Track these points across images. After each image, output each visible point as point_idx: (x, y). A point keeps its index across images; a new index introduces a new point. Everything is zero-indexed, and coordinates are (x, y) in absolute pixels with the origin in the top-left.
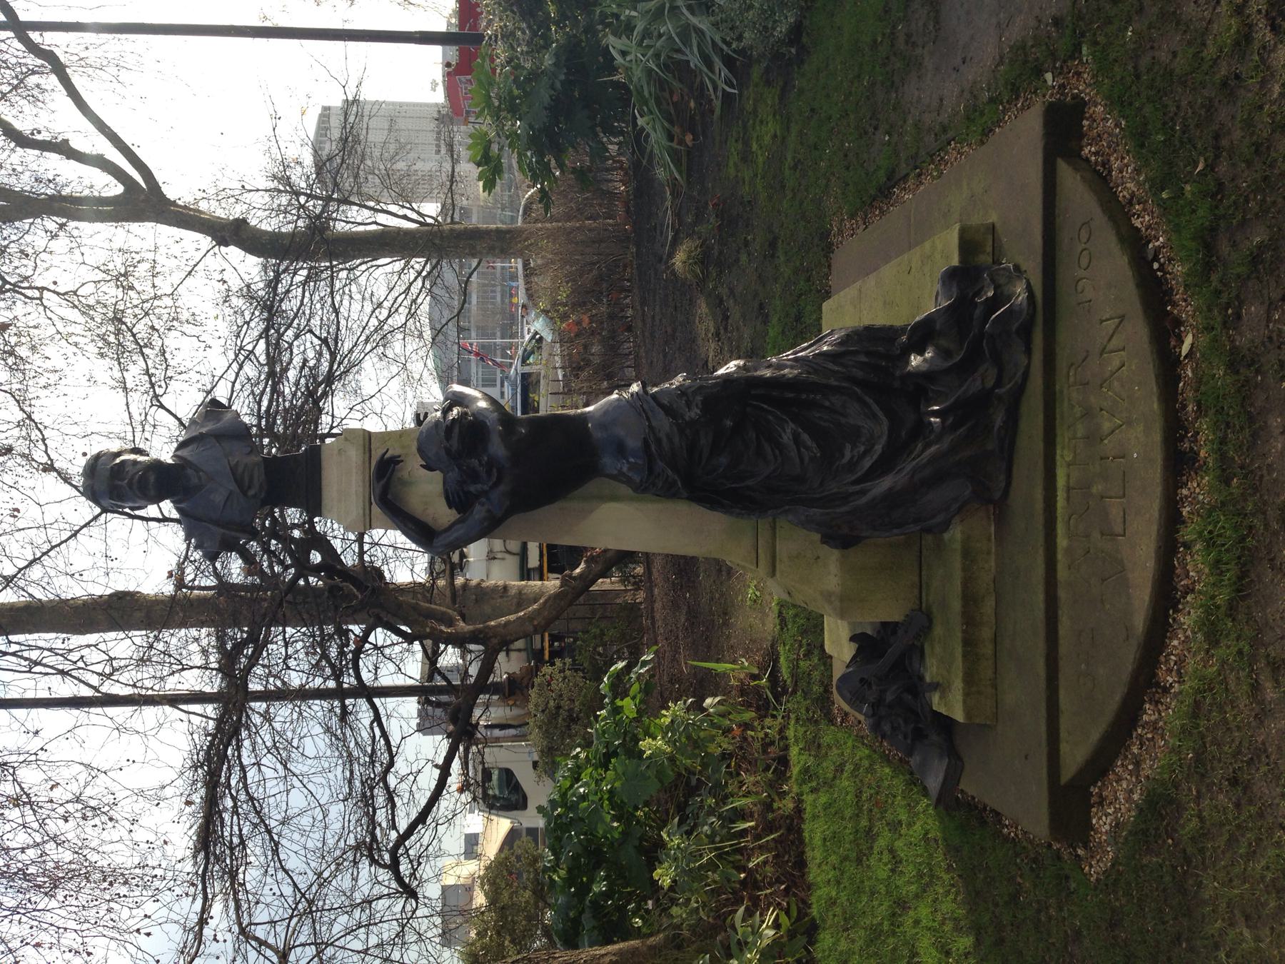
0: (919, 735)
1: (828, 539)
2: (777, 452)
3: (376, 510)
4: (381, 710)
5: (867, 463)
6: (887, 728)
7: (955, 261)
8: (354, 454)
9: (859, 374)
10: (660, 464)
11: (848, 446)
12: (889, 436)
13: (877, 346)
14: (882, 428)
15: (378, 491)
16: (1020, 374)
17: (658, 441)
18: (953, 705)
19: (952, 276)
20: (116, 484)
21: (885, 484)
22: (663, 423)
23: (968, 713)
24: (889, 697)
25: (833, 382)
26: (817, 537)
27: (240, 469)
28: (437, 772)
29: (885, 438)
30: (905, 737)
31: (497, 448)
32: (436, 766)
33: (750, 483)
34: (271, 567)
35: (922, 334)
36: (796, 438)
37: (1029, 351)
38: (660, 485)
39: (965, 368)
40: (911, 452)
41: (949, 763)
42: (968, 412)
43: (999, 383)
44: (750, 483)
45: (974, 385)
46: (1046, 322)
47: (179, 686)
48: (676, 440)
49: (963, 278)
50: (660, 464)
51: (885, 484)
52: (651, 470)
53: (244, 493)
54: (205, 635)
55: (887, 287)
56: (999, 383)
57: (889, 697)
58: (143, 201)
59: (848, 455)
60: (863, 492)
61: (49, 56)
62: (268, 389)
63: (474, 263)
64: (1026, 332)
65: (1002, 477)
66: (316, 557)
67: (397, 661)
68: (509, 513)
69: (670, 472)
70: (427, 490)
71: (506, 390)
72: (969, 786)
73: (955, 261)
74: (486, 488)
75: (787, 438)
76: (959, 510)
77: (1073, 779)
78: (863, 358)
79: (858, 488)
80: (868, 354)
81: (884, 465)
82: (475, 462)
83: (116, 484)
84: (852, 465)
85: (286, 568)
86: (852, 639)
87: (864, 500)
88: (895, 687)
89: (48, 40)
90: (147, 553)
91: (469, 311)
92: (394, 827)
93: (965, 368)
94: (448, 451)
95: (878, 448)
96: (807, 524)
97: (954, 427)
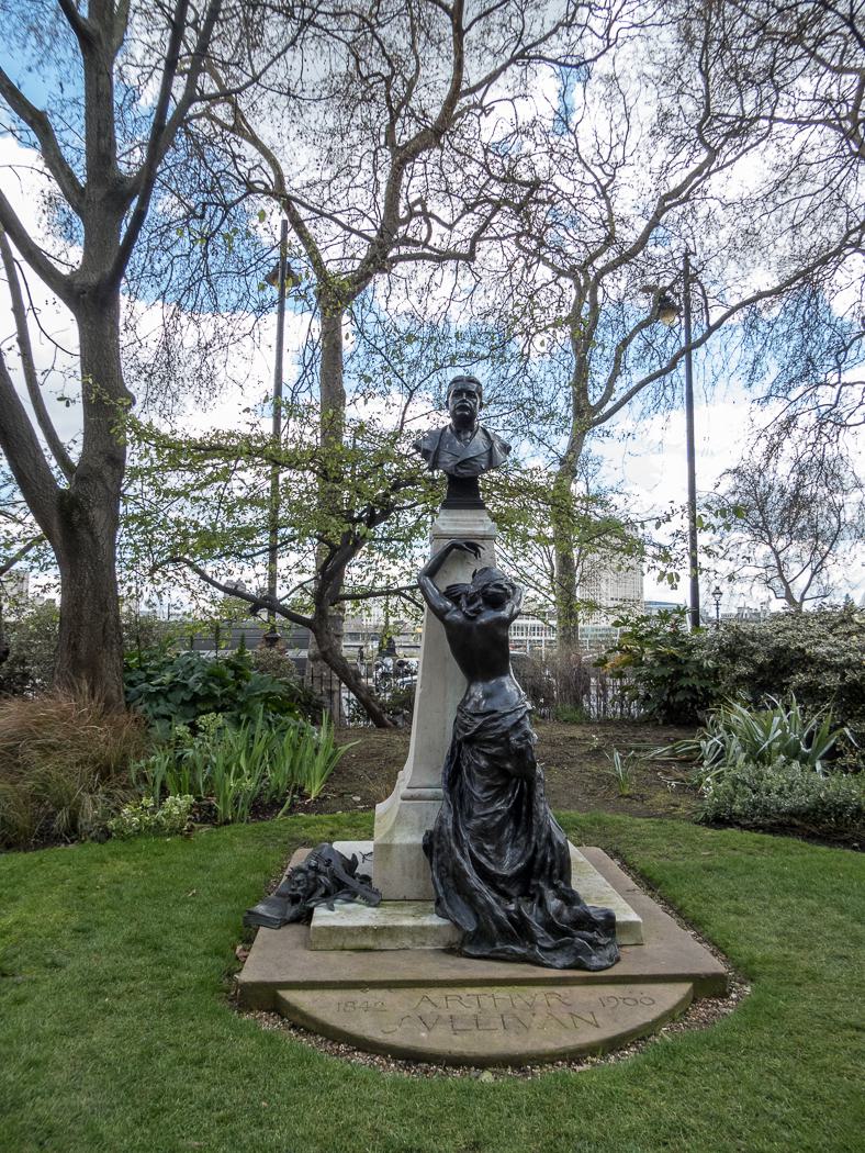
3: (447, 542)
5: (483, 859)
6: (300, 877)
9: (539, 856)
10: (479, 721)
11: (493, 848)
13: (556, 869)
14: (506, 871)
15: (459, 542)
17: (495, 720)
18: (323, 917)
19: (610, 917)
21: (467, 866)
22: (509, 721)
23: (315, 928)
24: (322, 878)
25: (533, 838)
26: (431, 826)
31: (488, 616)
33: (467, 781)
35: (570, 899)
36: (498, 812)
37: (565, 968)
39: (549, 926)
43: (543, 949)
45: (539, 932)
46: (588, 978)
48: (499, 731)
50: (479, 721)
52: (475, 715)
55: (596, 883)
56: (543, 949)
57: (322, 878)
58: (586, 416)
59: (488, 847)
61: (673, 365)
64: (579, 966)
65: (478, 953)
67: (297, 569)
75: (498, 806)
76: (456, 924)
79: (467, 853)
80: (553, 862)
82: (481, 601)
84: (481, 850)
86: (354, 856)
87: (459, 857)
89: (682, 369)
96: (441, 820)
97: (511, 919)
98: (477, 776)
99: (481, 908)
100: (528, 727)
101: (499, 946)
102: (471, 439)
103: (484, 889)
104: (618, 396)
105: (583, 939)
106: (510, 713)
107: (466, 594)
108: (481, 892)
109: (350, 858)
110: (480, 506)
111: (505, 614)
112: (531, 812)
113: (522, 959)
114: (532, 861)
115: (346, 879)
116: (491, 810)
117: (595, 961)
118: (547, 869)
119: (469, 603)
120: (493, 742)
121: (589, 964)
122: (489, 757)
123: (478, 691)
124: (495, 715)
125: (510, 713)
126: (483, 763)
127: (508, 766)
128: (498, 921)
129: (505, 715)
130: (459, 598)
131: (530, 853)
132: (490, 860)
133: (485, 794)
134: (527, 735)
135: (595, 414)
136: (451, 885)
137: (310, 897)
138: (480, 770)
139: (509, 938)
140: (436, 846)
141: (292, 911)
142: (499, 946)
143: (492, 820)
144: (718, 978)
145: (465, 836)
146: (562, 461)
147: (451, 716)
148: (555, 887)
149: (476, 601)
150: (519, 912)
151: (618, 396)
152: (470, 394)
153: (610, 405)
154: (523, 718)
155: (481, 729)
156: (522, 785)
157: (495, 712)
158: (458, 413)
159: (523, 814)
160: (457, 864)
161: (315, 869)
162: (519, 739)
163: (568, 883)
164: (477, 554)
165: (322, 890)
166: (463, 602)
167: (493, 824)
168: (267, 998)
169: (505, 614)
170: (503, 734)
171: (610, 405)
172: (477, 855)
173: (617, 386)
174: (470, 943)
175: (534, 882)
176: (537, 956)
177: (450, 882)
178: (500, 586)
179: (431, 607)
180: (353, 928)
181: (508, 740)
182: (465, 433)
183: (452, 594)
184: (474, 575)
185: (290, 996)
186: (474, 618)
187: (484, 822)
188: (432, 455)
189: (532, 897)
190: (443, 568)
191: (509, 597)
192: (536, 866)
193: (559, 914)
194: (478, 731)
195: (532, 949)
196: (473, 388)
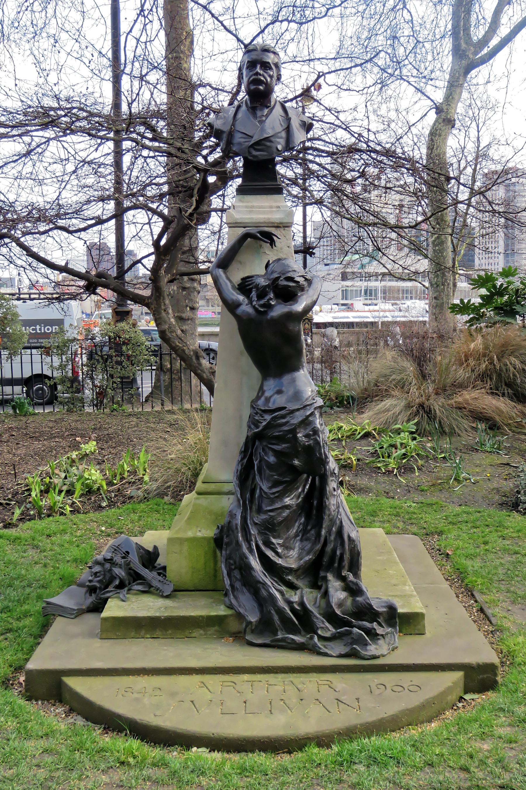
0: (92, 590)
1: (221, 529)
2: (277, 495)
3: (241, 231)
4: (106, 225)
5: (270, 554)
7: (400, 610)
8: (277, 217)
10: (268, 417)
12: (287, 568)
16: (326, 651)
17: (283, 417)
19: (392, 609)
20: (258, 69)
21: (255, 563)
22: (298, 417)
25: (323, 532)
26: (223, 521)
27: (268, 144)
28: (63, 264)
29: (286, 565)
30: (90, 581)
31: (279, 310)
32: (67, 263)
34: (206, 148)
35: (354, 591)
36: (287, 507)
38: (256, 418)
39: (331, 617)
40: (276, 582)
41: (74, 610)
42: (304, 620)
44: (257, 478)
47: (199, 651)
48: (286, 428)
49: (393, 617)
50: (268, 417)
51: (255, 563)
52: (265, 411)
53: (252, 146)
54: (162, 98)
55: (391, 568)
56: (321, 638)
60: (251, 551)
62: (317, 160)
63: (427, 284)
64: (352, 654)
66: (212, 179)
67: (142, 235)
68: (238, 318)
69: (264, 423)
70: (254, 266)
71: (450, 255)
72: (59, 624)
73: (400, 610)
74: (254, 303)
75: (288, 501)
77: (66, 685)
78: (338, 553)
80: (342, 555)
81: (269, 565)
83: (258, 69)
84: (268, 544)
85: (205, 158)
86: (155, 547)
88: (123, 574)
90: (217, 69)
91: (393, 280)
92: (24, 234)
93: (331, 617)
94: (277, 279)
95: (279, 561)
97: (293, 610)
98: (268, 472)
99: (264, 599)
100: (318, 422)
101: (280, 636)
102: (267, 116)
103: (268, 581)
104: (504, 31)
105: (363, 627)
106: (298, 410)
107: (257, 286)
108: (264, 584)
109: (151, 549)
110: (278, 191)
111: (299, 307)
112: (322, 507)
113: (300, 648)
114: (322, 552)
115: (145, 572)
116: (278, 505)
117: (372, 649)
118: (333, 558)
119: (260, 297)
120: (280, 439)
121: (363, 652)
122: (276, 453)
123: (271, 385)
124: (283, 412)
125: (298, 410)
126: (272, 459)
127: (296, 462)
128: (280, 612)
129: (293, 412)
130: (250, 291)
131: (319, 547)
132: (277, 553)
133: (274, 490)
134: (316, 432)
135: (481, 49)
136: (238, 577)
137: (107, 587)
138: (269, 466)
139: (291, 628)
140: (226, 540)
141: (91, 600)
142: (280, 636)
143: (279, 514)
144: (491, 668)
145: (254, 531)
146: (439, 110)
147: (247, 412)
148: (343, 579)
149: (266, 295)
150: (302, 604)
151: (504, 31)
152: (266, 66)
153: (494, 42)
154: (312, 414)
155: (269, 426)
156: (313, 481)
157: (284, 408)
158: (252, 87)
159: (314, 506)
160: (244, 557)
161: (110, 561)
162: (307, 436)
163: (356, 574)
164: (272, 243)
165: (117, 582)
166: (254, 294)
167: (280, 519)
168: (50, 688)
169: (299, 307)
170: (289, 431)
171: (494, 42)
172: (263, 548)
173: (504, 19)
174: (253, 631)
175: (322, 574)
176: (315, 645)
177: (237, 574)
178: (291, 279)
179: (225, 301)
180: (144, 618)
181: (295, 438)
182: (262, 110)
183: (245, 286)
184: (267, 266)
185: (75, 683)
186: (265, 313)
187: (271, 517)
188: (225, 136)
189: (319, 588)
190: (239, 257)
191: (302, 289)
192: (326, 559)
193: (340, 605)
194: (266, 427)
195: (312, 638)
196: (270, 58)
